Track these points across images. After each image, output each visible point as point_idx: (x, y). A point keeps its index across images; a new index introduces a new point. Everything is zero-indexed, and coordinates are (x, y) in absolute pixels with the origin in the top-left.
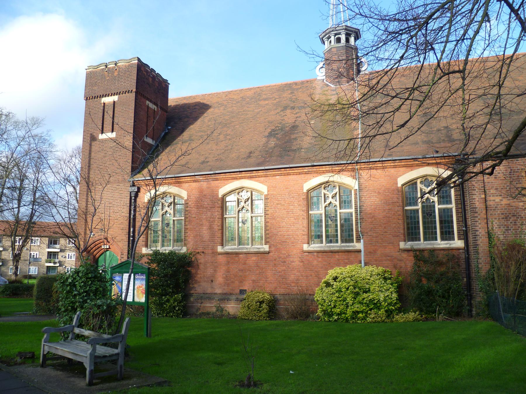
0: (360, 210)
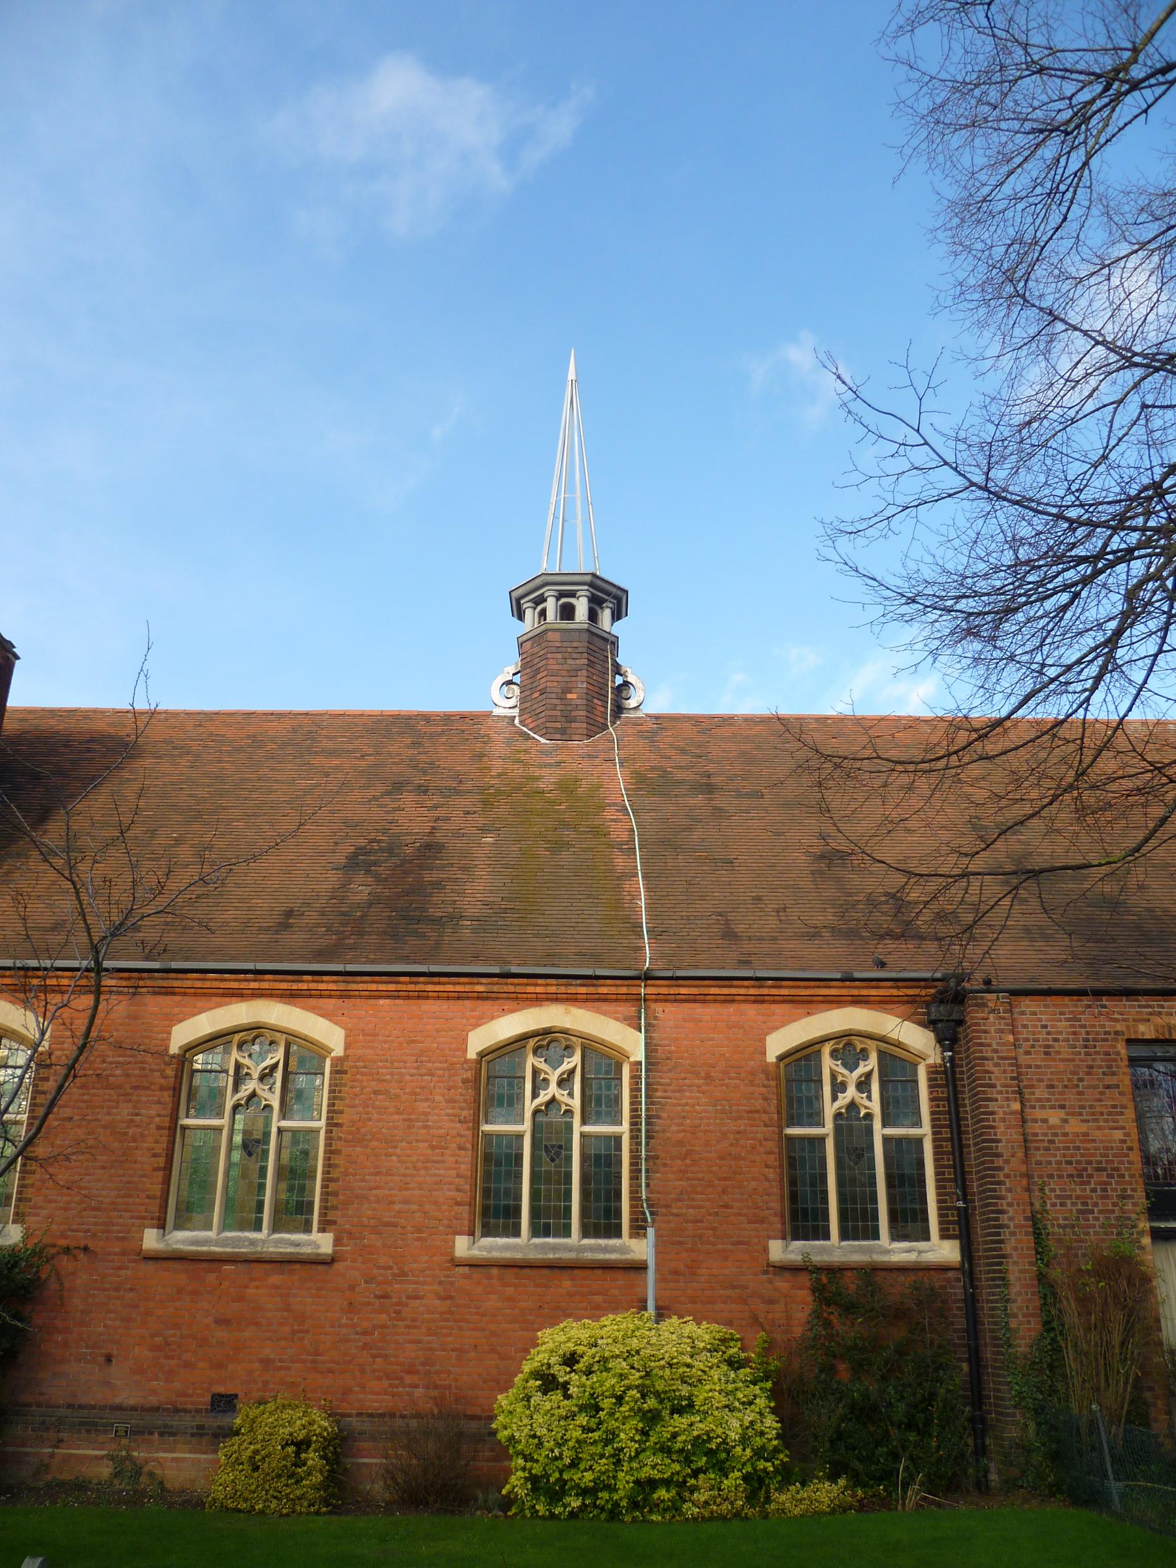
0: (648, 1128)
